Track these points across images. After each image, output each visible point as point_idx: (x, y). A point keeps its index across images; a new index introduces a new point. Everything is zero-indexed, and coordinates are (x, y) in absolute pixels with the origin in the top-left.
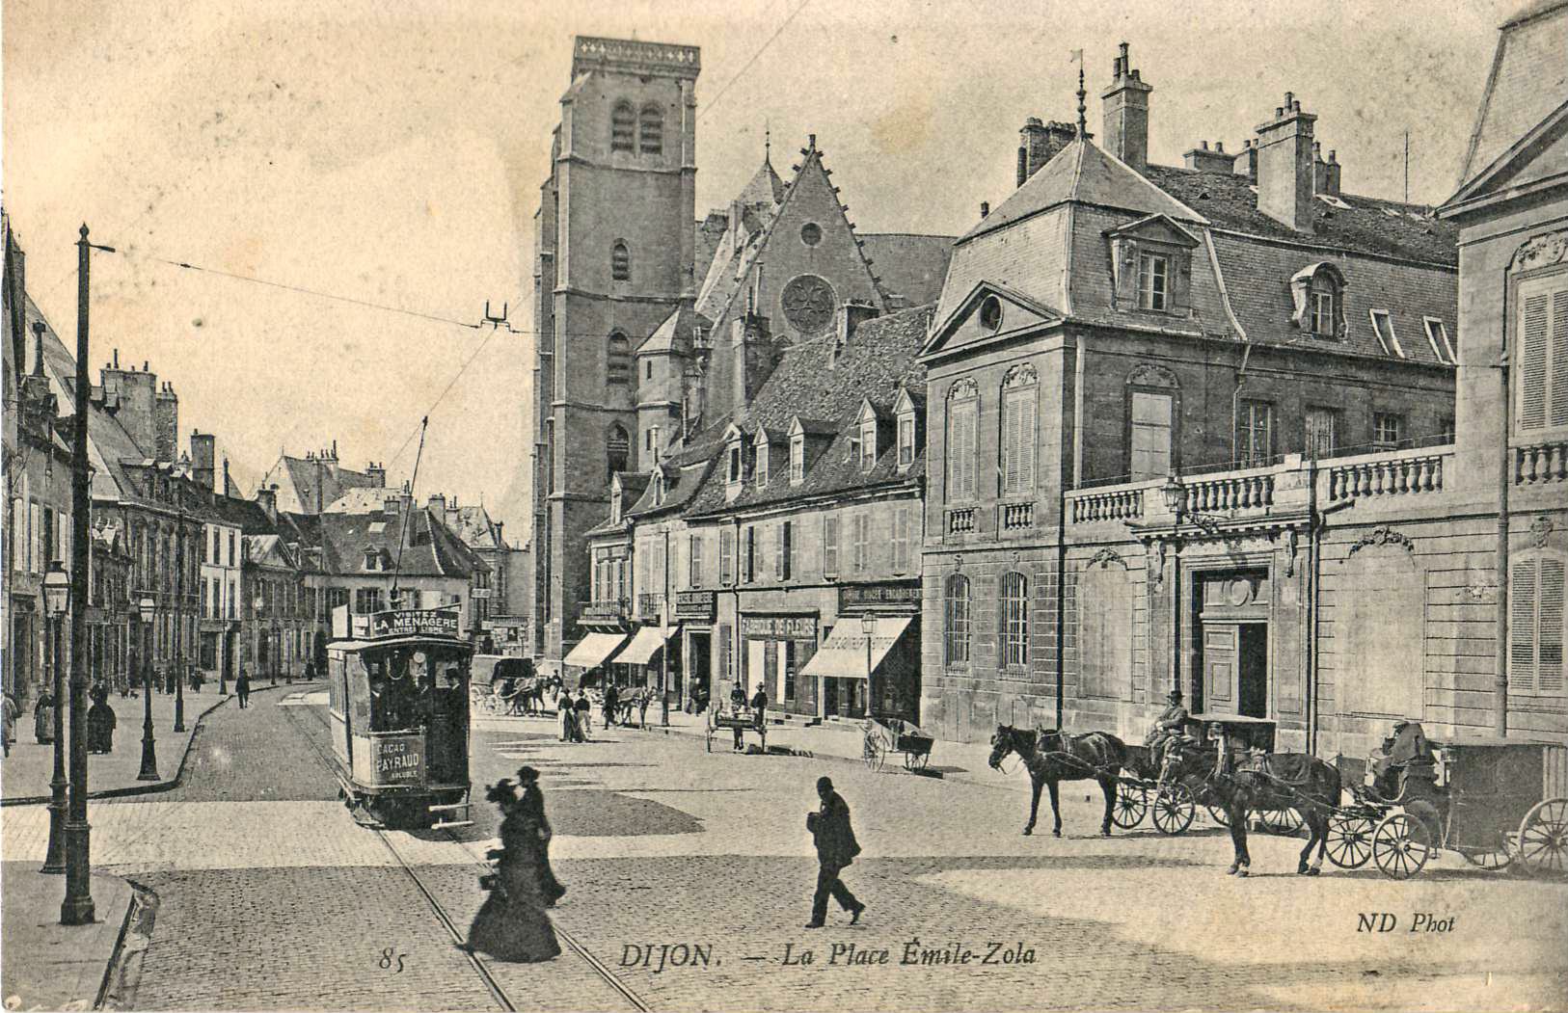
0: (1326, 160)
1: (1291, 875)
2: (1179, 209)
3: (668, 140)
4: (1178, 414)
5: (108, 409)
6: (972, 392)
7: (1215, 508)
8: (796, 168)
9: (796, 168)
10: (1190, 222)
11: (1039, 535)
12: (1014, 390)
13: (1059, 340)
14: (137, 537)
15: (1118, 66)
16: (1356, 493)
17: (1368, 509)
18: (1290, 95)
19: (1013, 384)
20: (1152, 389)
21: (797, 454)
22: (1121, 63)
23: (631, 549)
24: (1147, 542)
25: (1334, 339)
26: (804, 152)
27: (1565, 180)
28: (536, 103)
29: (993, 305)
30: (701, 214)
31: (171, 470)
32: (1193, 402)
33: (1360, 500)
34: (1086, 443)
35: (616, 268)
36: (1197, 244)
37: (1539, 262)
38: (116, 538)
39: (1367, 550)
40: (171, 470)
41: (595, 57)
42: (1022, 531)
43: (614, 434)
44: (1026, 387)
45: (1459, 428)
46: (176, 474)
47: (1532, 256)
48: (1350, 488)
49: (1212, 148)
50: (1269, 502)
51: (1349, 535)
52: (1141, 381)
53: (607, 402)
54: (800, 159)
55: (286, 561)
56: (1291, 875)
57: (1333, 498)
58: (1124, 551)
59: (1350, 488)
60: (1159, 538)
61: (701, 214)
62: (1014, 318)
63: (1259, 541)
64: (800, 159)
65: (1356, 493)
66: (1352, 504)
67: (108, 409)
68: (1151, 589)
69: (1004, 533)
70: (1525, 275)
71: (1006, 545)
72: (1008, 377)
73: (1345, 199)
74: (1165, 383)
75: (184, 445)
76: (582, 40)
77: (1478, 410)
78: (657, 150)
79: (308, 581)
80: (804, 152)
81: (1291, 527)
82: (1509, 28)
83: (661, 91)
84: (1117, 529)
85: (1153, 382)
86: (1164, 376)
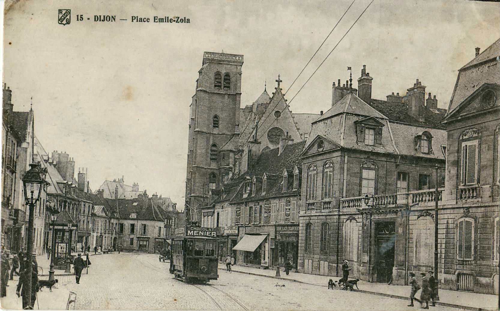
0: (433, 98)
1: (273, 277)
2: (377, 114)
3: (232, 86)
4: (377, 175)
5: (49, 163)
6: (315, 168)
7: (381, 204)
8: (273, 93)
9: (273, 93)
10: (382, 119)
11: (333, 212)
12: (328, 168)
13: (339, 154)
14: (61, 205)
15: (362, 72)
16: (419, 201)
17: (422, 206)
18: (418, 80)
19: (327, 166)
20: (369, 169)
21: (264, 186)
22: (363, 71)
23: (214, 212)
24: (362, 214)
25: (428, 154)
26: (276, 88)
27: (499, 108)
28: (188, 78)
29: (322, 142)
30: (243, 106)
31: (72, 184)
32: (382, 172)
33: (420, 203)
34: (348, 185)
35: (214, 124)
36: (384, 125)
37: (467, 137)
38: (54, 206)
39: (421, 218)
40: (72, 184)
41: (211, 60)
42: (327, 210)
43: (212, 176)
44: (314, 170)
45: (446, 183)
46: (73, 186)
47: (465, 135)
48: (418, 200)
49: (395, 94)
50: (396, 203)
51: (417, 213)
52: (365, 166)
53: (210, 166)
54: (274, 91)
55: (106, 214)
56: (273, 277)
57: (413, 202)
58: (356, 217)
59: (418, 200)
60: (365, 213)
61: (243, 106)
62: (327, 146)
63: (382, 215)
64: (274, 91)
65: (419, 201)
66: (418, 204)
67: (49, 163)
68: (363, 228)
69: (323, 211)
70: (464, 140)
71: (323, 214)
72: (325, 164)
73: (439, 110)
74: (372, 166)
75: (76, 176)
76: (207, 53)
77: (450, 178)
78: (229, 87)
79: (112, 221)
80: (276, 88)
81: (365, 213)
82: (462, 70)
83: (231, 69)
84: (353, 210)
85: (369, 166)
86: (373, 165)
